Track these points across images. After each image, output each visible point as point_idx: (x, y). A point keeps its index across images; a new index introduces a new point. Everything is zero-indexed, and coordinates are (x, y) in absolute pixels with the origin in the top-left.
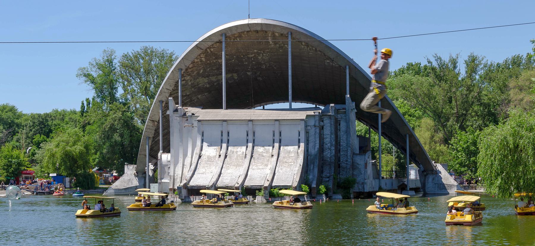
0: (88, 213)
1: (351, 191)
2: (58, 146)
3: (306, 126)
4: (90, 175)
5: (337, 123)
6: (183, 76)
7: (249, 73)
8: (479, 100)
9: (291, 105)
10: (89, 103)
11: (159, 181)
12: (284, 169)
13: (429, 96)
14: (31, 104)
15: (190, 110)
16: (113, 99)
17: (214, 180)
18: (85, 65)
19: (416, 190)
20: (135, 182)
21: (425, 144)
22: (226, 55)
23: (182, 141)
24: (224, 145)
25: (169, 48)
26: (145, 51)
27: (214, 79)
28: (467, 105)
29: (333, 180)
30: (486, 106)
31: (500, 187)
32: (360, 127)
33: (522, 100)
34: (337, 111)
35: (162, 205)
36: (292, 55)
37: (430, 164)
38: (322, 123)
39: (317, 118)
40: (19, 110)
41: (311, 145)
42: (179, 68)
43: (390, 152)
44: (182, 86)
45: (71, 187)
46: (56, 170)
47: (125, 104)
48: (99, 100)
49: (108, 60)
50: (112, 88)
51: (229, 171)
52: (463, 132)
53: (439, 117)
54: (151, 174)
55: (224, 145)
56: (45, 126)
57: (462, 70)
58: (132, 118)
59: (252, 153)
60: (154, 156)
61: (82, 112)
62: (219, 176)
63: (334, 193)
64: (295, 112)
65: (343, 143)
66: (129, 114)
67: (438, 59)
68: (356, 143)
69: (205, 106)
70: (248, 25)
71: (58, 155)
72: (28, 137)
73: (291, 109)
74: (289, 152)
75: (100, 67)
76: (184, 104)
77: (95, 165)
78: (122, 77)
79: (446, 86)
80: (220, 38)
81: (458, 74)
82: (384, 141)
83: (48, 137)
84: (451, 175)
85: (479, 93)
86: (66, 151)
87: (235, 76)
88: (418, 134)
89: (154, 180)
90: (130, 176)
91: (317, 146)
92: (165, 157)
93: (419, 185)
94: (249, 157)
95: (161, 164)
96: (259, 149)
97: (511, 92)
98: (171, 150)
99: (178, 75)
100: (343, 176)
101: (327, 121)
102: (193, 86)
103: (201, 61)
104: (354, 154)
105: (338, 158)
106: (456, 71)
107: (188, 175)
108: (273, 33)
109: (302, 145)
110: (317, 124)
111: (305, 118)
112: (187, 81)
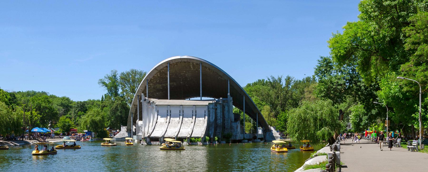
0: (41, 152)
1: (230, 139)
2: (88, 117)
3: (208, 108)
4: (104, 131)
5: (223, 107)
6: (148, 83)
7: (181, 83)
8: (291, 97)
9: (201, 98)
10: (105, 97)
11: (137, 134)
12: (197, 129)
13: (269, 95)
14: (77, 97)
15: (152, 100)
16: (116, 94)
17: (163, 134)
18: (102, 77)
19: (261, 139)
20: (126, 135)
21: (266, 117)
22: (170, 73)
23: (148, 115)
24: (169, 117)
25: (139, 68)
26: (132, 71)
27: (164, 85)
28: (286, 99)
29: (220, 134)
30: (294, 100)
31: (297, 137)
32: (235, 109)
33: (310, 97)
34: (223, 101)
35: (74, 146)
36: (202, 74)
37: (268, 127)
38: (216, 107)
39: (214, 105)
40: (71, 100)
41: (211, 117)
42: (147, 80)
43: (250, 122)
44: (148, 88)
45: (95, 137)
46: (87, 128)
47: (122, 97)
48: (110, 95)
49: (114, 76)
50: (116, 89)
51: (170, 130)
52: (284, 112)
53: (273, 106)
54: (134, 131)
55: (169, 117)
56: (83, 107)
57: (284, 83)
58: (126, 104)
59: (182, 121)
60: (135, 123)
61: (102, 100)
62: (166, 132)
63: (222, 140)
64: (205, 101)
65: (226, 117)
66: (125, 102)
67: (273, 78)
68: (233, 117)
69: (159, 98)
70: (181, 59)
71: (88, 122)
72: (75, 113)
73: (201, 100)
74: (200, 121)
75: (110, 78)
76: (149, 97)
77: (108, 126)
78: (121, 84)
79: (276, 91)
80: (167, 65)
81: (282, 85)
82: (247, 116)
83: (85, 113)
84: (277, 132)
85: (292, 94)
86: (92, 119)
87: (175, 84)
88: (262, 113)
89: (135, 134)
90: (123, 132)
91: (214, 118)
92: (140, 123)
93: (263, 137)
94: (180, 123)
95: (138, 126)
96: (186, 119)
97: (305, 94)
98: (143, 119)
99: (146, 83)
100: (226, 132)
101: (219, 106)
102: (154, 88)
103: (158, 76)
104: (232, 122)
105: (224, 123)
106: (281, 83)
107: (150, 131)
108: (193, 63)
109: (206, 117)
110: (214, 107)
111: (207, 104)
112: (151, 86)
